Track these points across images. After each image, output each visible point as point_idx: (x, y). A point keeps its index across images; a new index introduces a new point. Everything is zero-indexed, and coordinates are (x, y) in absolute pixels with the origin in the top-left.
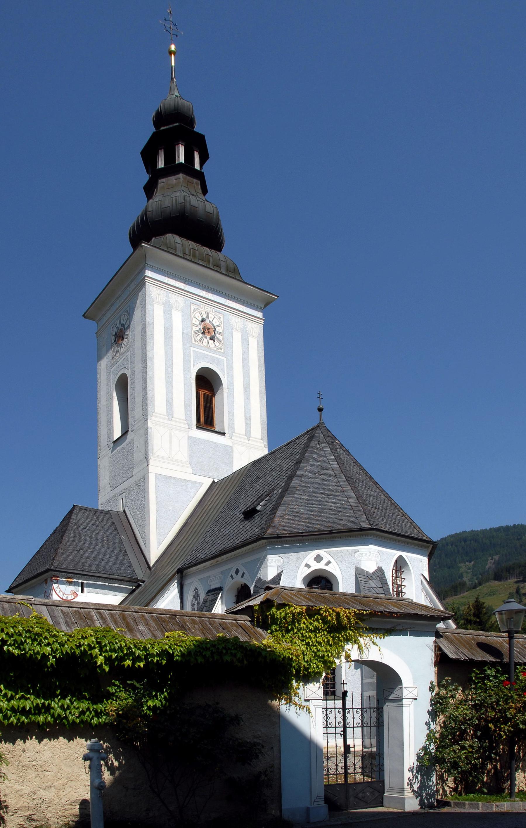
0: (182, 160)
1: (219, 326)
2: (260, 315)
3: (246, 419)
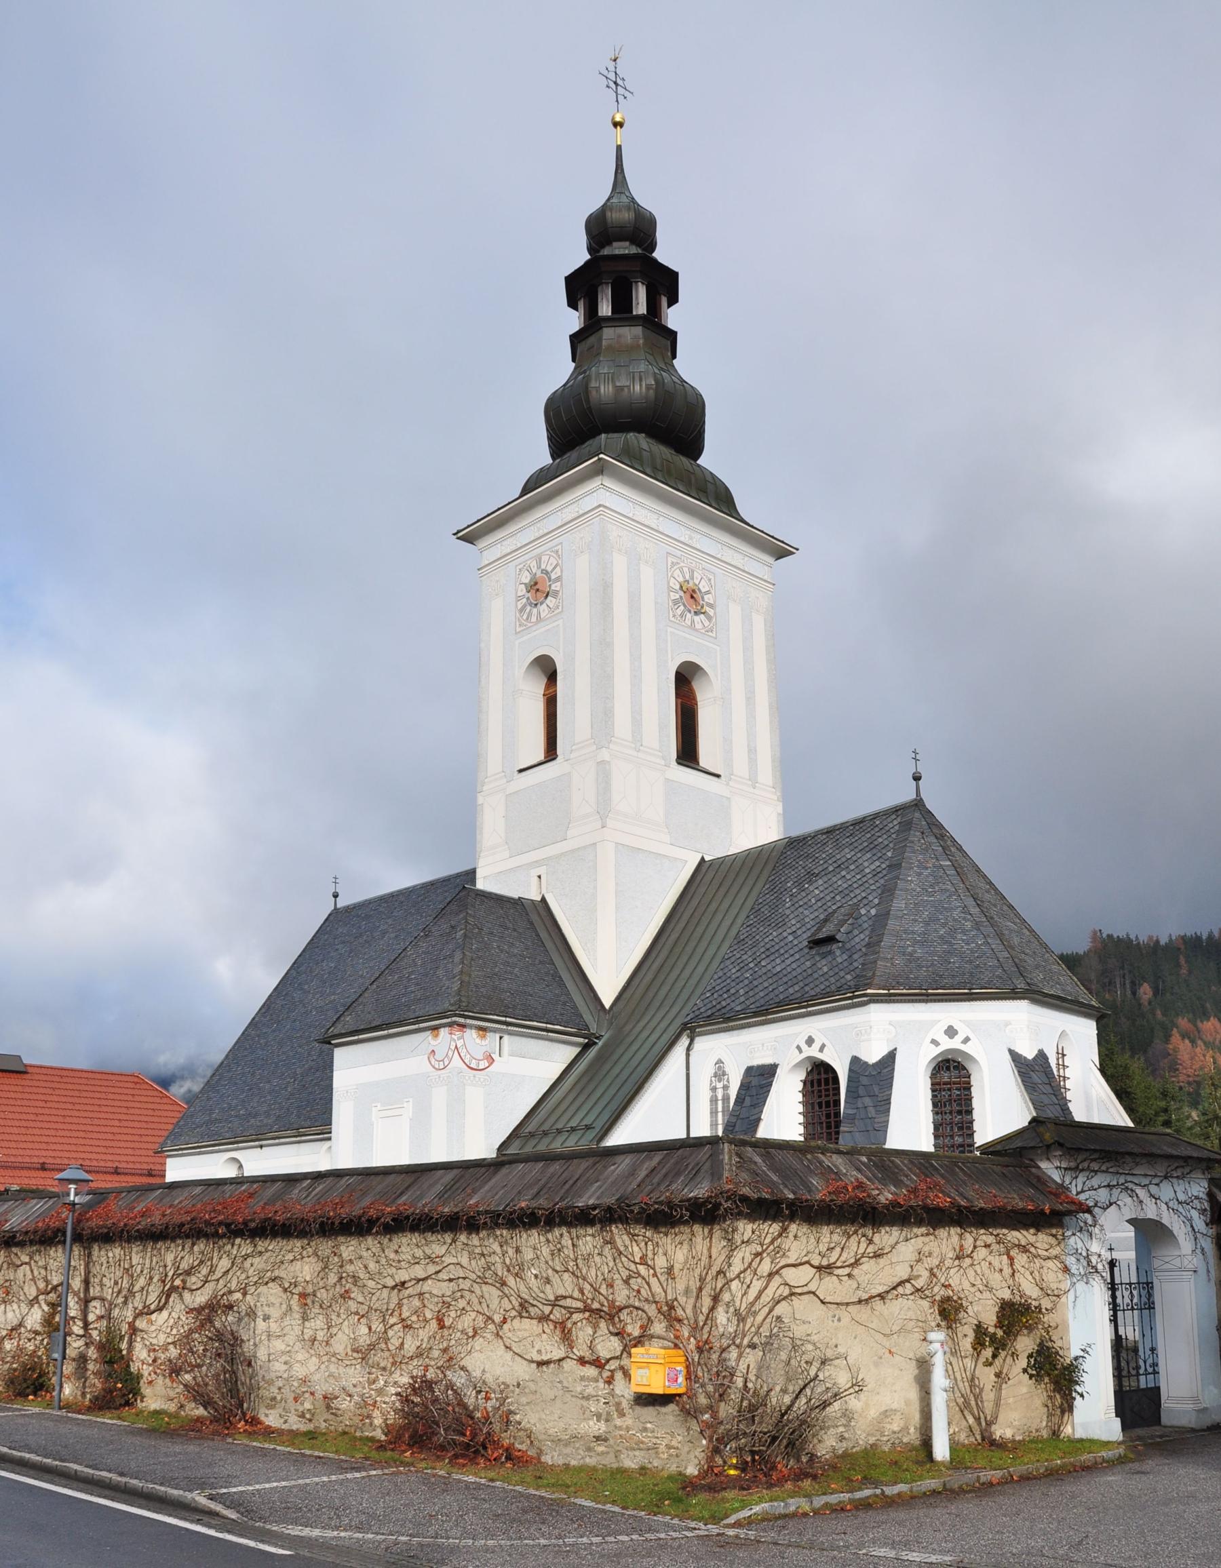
1: (708, 592)
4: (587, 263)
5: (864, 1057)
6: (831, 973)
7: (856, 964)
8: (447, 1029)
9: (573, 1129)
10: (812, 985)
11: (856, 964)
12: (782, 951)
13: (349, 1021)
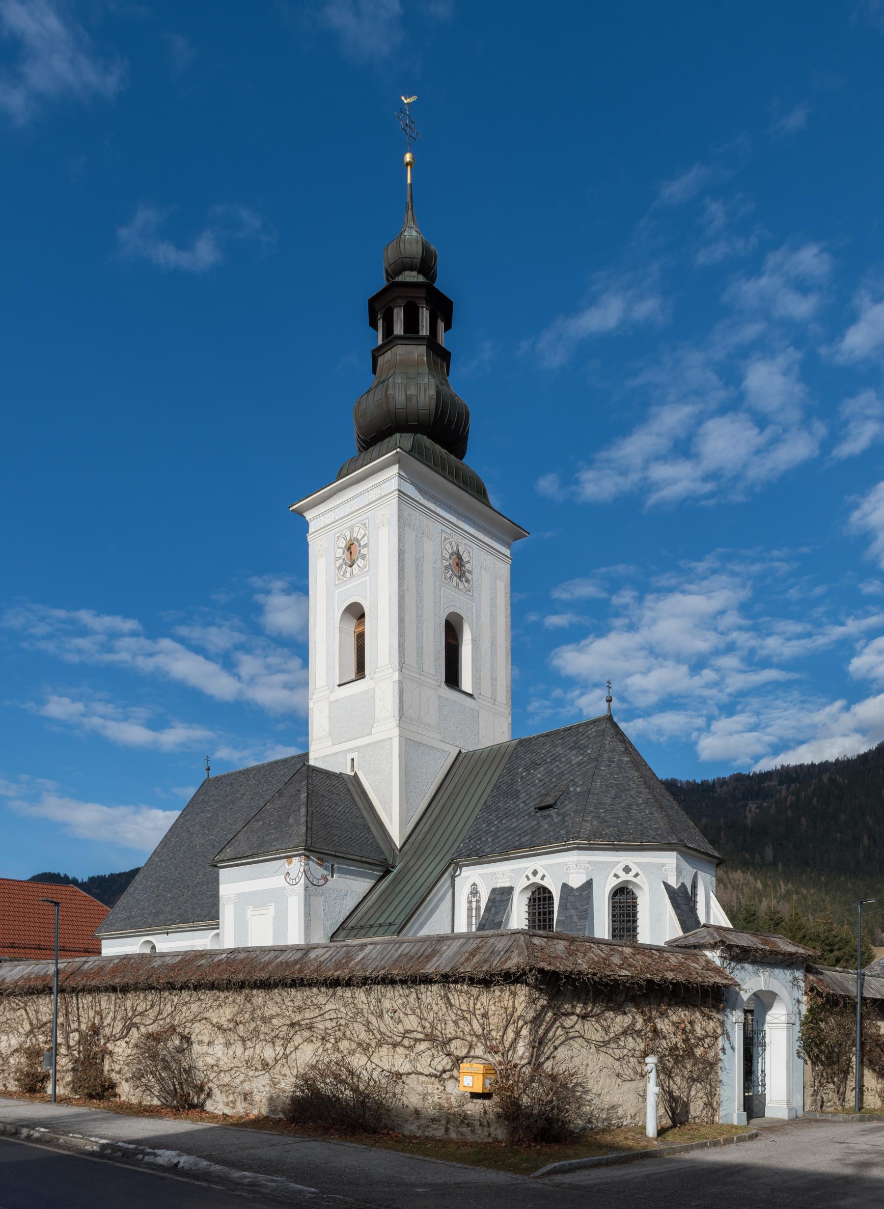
2: (507, 552)
3: (492, 679)
6: (550, 829)
8: (298, 858)
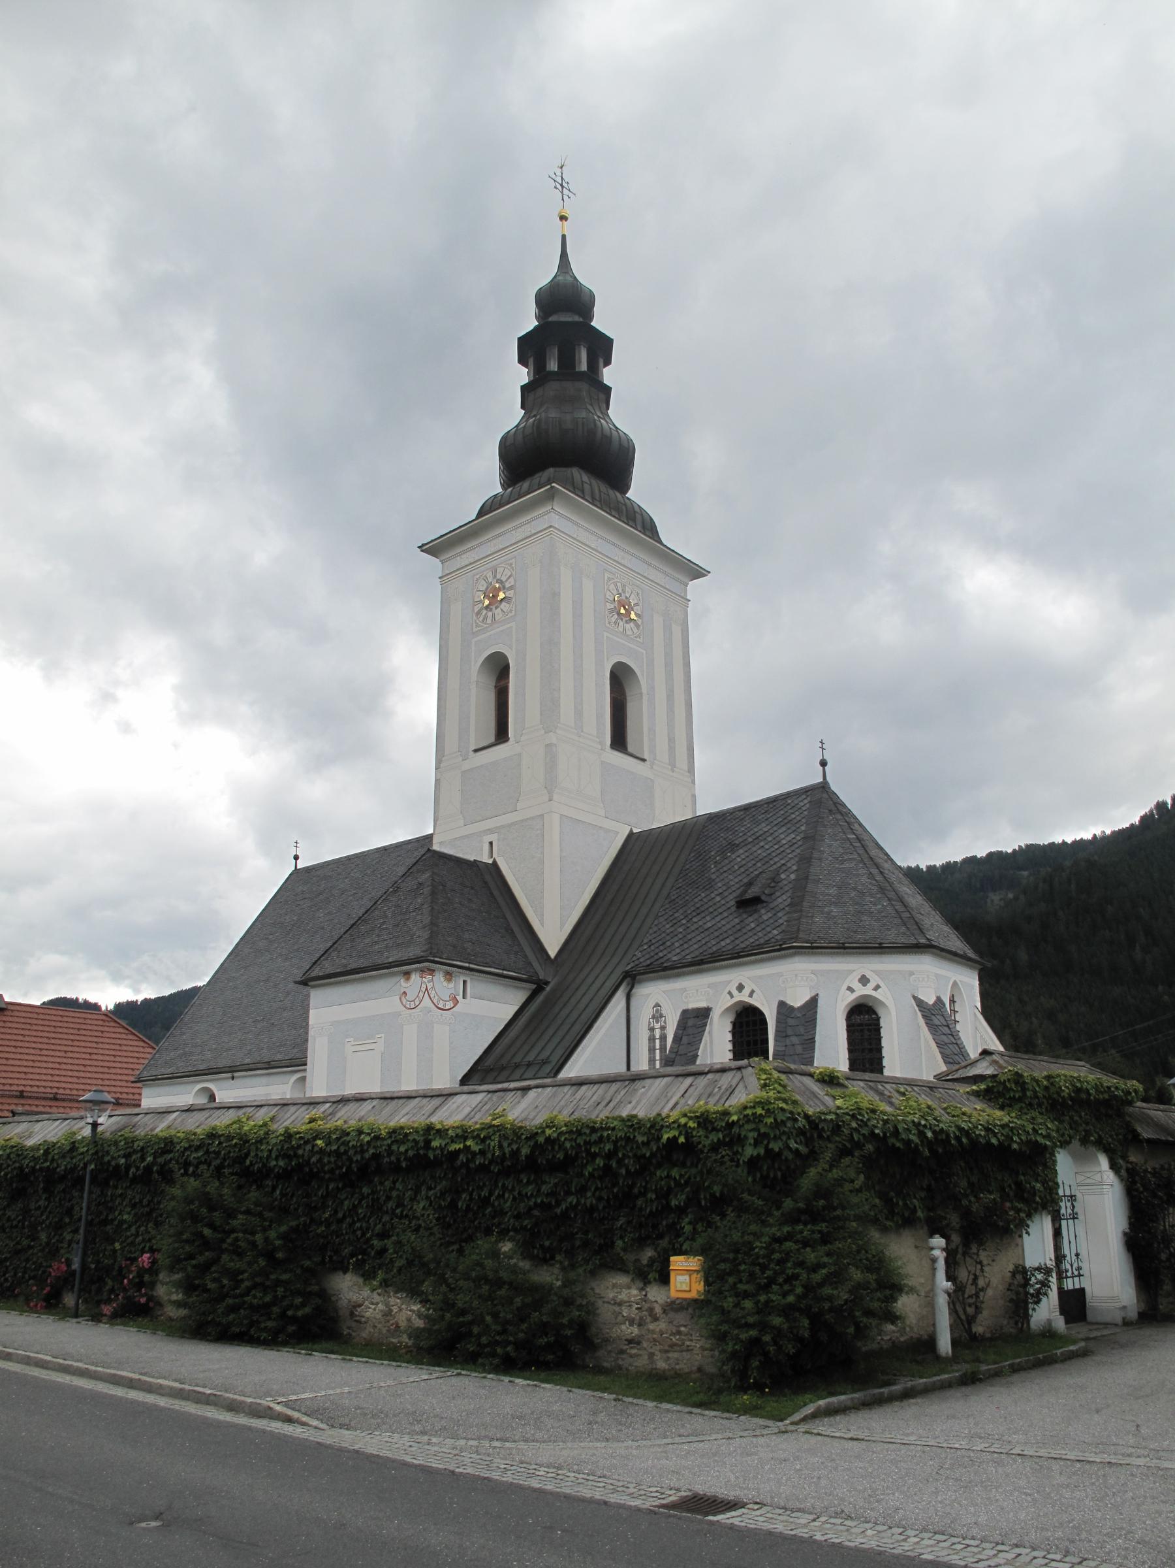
0: (584, 367)
3: (670, 740)
4: (536, 328)
5: (790, 1002)
7: (781, 921)
9: (529, 1065)
10: (742, 939)
11: (781, 921)
12: (711, 910)
13: (328, 967)
